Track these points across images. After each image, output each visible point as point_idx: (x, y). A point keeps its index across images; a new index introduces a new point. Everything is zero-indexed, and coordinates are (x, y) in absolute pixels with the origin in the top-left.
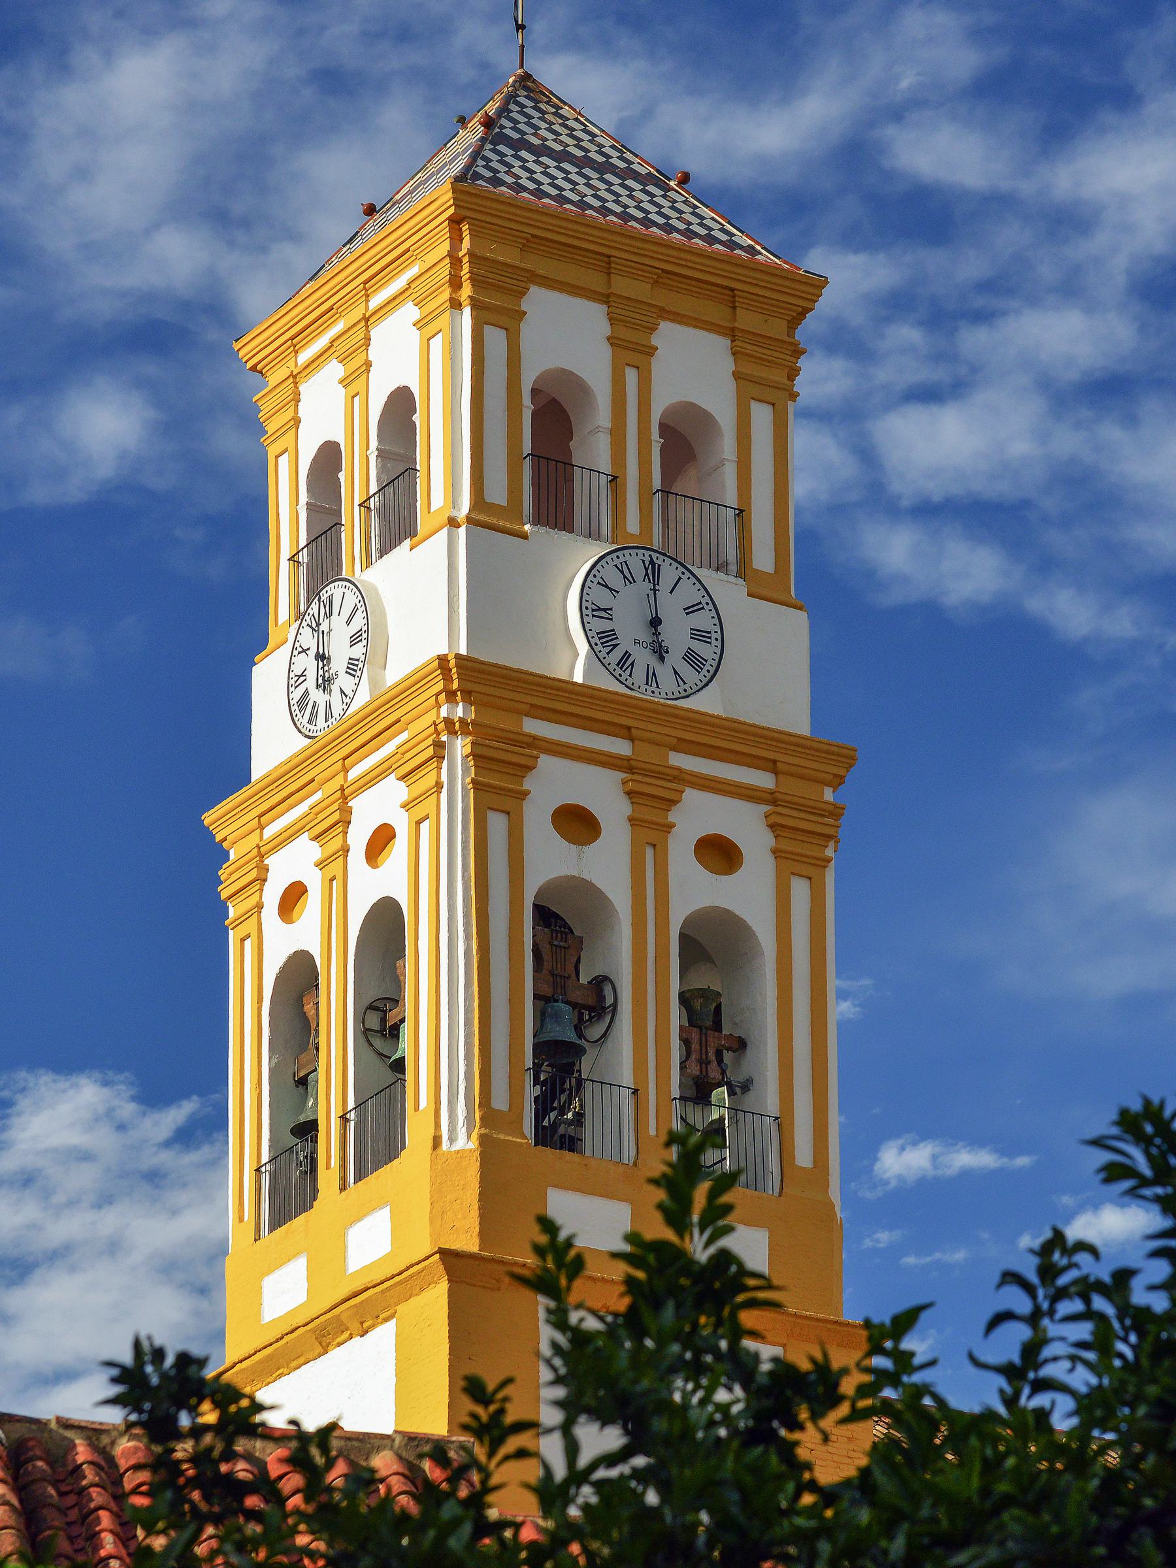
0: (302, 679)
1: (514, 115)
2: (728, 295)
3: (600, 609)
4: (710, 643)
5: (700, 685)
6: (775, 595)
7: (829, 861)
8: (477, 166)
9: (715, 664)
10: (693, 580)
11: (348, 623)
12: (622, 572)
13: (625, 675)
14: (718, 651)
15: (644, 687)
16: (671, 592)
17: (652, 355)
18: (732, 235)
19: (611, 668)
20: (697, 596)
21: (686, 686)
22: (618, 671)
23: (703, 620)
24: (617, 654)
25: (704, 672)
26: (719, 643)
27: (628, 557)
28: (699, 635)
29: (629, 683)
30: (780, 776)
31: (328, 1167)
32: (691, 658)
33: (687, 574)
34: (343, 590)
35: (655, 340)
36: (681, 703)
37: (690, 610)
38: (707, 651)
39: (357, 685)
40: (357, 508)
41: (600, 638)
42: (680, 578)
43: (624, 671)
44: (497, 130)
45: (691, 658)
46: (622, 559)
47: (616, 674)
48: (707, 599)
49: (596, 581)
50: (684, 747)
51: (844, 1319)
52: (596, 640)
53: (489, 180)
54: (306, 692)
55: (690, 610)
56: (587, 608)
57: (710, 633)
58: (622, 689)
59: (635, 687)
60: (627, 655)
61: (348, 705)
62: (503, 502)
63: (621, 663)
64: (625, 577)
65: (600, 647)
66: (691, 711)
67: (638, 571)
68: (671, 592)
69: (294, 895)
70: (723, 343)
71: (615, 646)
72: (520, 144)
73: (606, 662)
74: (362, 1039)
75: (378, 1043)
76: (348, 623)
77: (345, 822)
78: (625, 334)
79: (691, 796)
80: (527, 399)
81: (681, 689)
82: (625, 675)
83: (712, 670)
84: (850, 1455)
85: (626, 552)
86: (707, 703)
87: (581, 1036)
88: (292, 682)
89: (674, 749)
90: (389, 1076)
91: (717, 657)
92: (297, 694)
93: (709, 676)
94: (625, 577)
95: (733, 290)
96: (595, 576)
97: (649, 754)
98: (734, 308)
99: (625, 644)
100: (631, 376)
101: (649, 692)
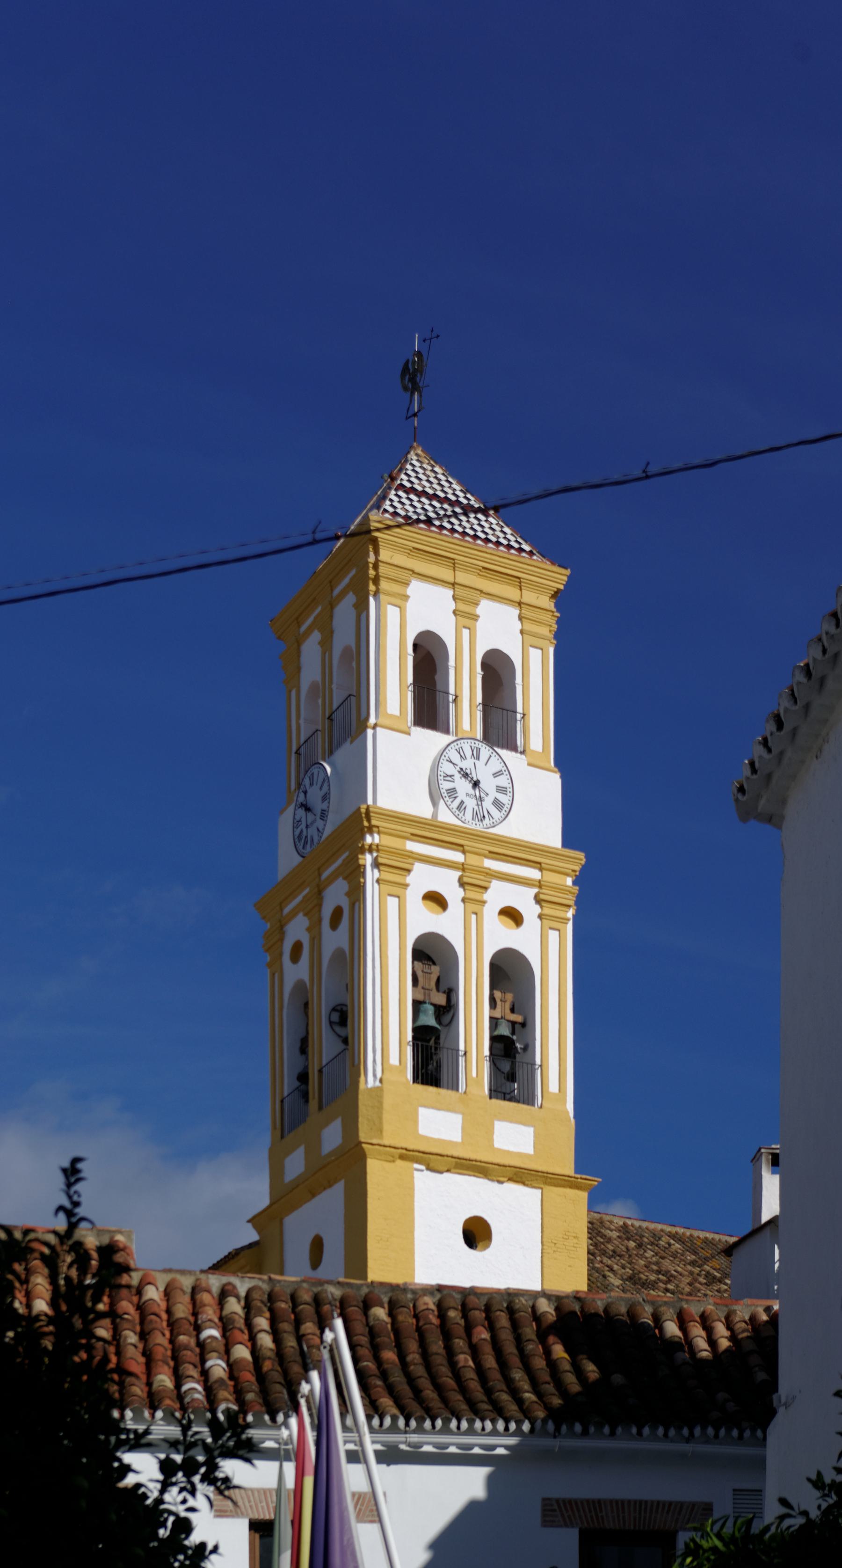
0: (300, 823)
1: (410, 472)
2: (451, 563)
3: (447, 776)
4: (506, 794)
5: (501, 819)
6: (542, 764)
7: (568, 920)
8: (386, 505)
9: (509, 807)
10: (497, 757)
11: (321, 788)
12: (459, 753)
13: (461, 815)
14: (511, 799)
15: (471, 821)
16: (486, 764)
17: (476, 620)
18: (520, 543)
19: (453, 811)
20: (498, 767)
21: (494, 821)
22: (457, 812)
23: (503, 781)
24: (457, 802)
25: (503, 811)
26: (511, 794)
27: (463, 745)
28: (501, 790)
29: (463, 819)
30: (467, 854)
31: (314, 1098)
32: (497, 804)
33: (494, 753)
34: (318, 770)
35: (479, 611)
36: (491, 830)
37: (496, 775)
38: (504, 799)
39: (325, 825)
40: (327, 721)
41: (448, 793)
42: (490, 756)
43: (461, 813)
44: (399, 482)
45: (497, 804)
46: (460, 745)
47: (456, 814)
48: (505, 768)
49: (445, 759)
50: (494, 855)
51: (386, 1142)
52: (446, 794)
53: (449, 530)
54: (302, 831)
55: (496, 775)
56: (510, 792)
57: (506, 788)
58: (459, 823)
59: (467, 821)
60: (462, 802)
61: (321, 837)
62: (397, 713)
63: (459, 808)
64: (461, 756)
65: (447, 798)
66: (495, 835)
67: (468, 753)
68: (486, 764)
69: (297, 951)
70: (516, 612)
71: (456, 798)
72: (452, 504)
73: (451, 807)
74: (329, 1027)
75: (338, 1029)
76: (321, 788)
77: (320, 905)
78: (462, 607)
79: (418, 867)
80: (410, 649)
81: (491, 822)
82: (461, 815)
83: (508, 810)
84: (575, 1245)
85: (462, 741)
86: (506, 830)
87: (439, 1023)
88: (295, 825)
89: (486, 857)
90: (342, 1046)
91: (510, 803)
92: (297, 832)
93: (506, 814)
94: (461, 756)
95: (453, 559)
96: (445, 756)
97: (473, 860)
98: (521, 590)
99: (461, 796)
100: (466, 632)
101: (474, 825)
